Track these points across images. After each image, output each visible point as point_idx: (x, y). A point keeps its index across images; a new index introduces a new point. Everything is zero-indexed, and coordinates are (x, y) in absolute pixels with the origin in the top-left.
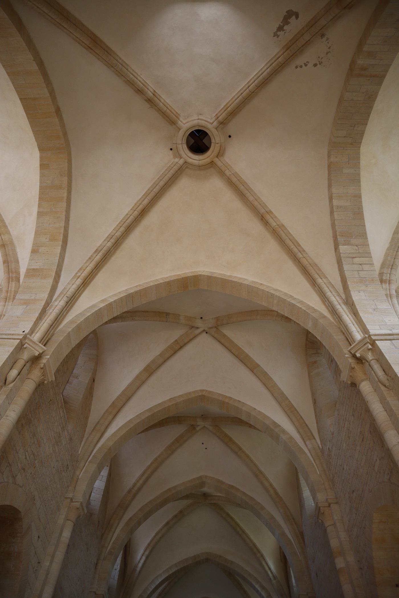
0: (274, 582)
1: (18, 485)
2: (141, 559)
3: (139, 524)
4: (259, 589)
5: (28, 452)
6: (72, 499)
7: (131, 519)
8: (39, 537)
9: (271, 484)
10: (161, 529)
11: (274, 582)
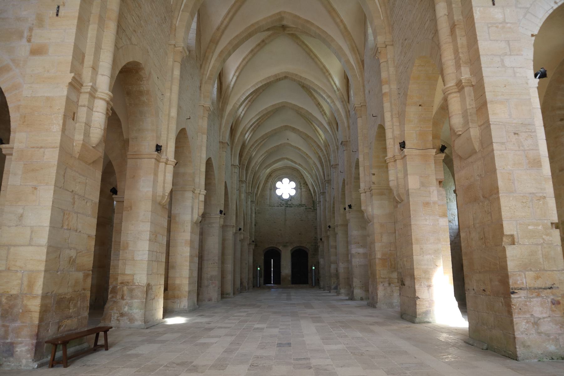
0: (337, 92)
1: (135, 44)
2: (233, 78)
3: (229, 55)
4: (326, 98)
5: (134, 16)
6: (175, 45)
7: (222, 51)
8: (158, 78)
9: (341, 20)
10: (247, 56)
11: (337, 92)
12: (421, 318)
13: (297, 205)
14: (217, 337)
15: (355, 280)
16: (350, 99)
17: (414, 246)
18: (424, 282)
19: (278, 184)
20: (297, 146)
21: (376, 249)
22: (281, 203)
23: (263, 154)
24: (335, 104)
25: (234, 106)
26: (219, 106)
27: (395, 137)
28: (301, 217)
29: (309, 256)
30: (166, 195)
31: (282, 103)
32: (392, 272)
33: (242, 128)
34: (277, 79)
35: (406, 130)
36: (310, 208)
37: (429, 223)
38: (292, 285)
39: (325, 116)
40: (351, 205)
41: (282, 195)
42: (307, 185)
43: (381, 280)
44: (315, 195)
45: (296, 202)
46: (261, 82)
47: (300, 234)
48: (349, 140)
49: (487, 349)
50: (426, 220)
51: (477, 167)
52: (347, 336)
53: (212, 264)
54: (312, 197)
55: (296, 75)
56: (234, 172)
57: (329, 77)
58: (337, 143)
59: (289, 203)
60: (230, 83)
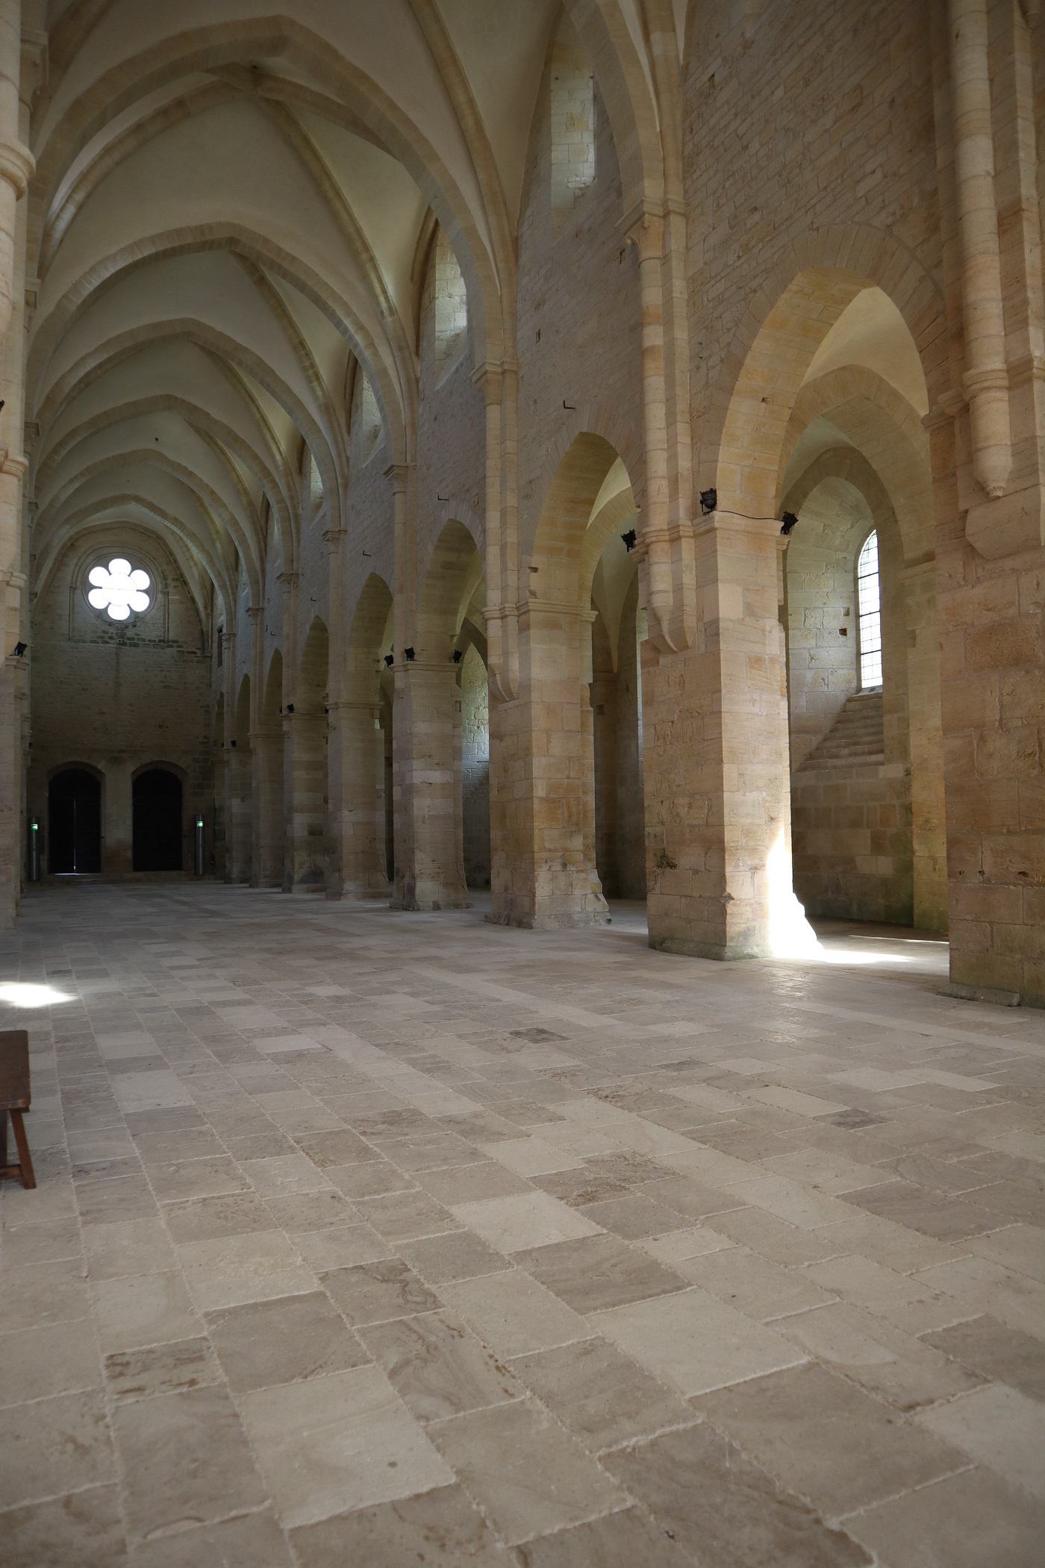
12: (736, 946)
13: (155, 641)
15: (419, 856)
17: (726, 767)
18: (744, 858)
19: (97, 575)
20: (184, 464)
21: (535, 774)
22: (105, 632)
23: (76, 477)
24: (376, 354)
25: (59, 305)
27: (679, 475)
28: (165, 677)
32: (572, 834)
34: (205, 243)
35: (720, 459)
36: (192, 652)
37: (760, 711)
38: (136, 873)
39: (315, 384)
40: (412, 649)
41: (107, 608)
42: (185, 583)
43: (545, 855)
44: (207, 615)
45: (152, 633)
46: (153, 239)
47: (161, 726)
48: (414, 464)
49: (1019, 1005)
50: (753, 702)
51: (1035, 582)
54: (200, 621)
55: (266, 241)
57: (368, 266)
59: (130, 633)
60: (54, 223)
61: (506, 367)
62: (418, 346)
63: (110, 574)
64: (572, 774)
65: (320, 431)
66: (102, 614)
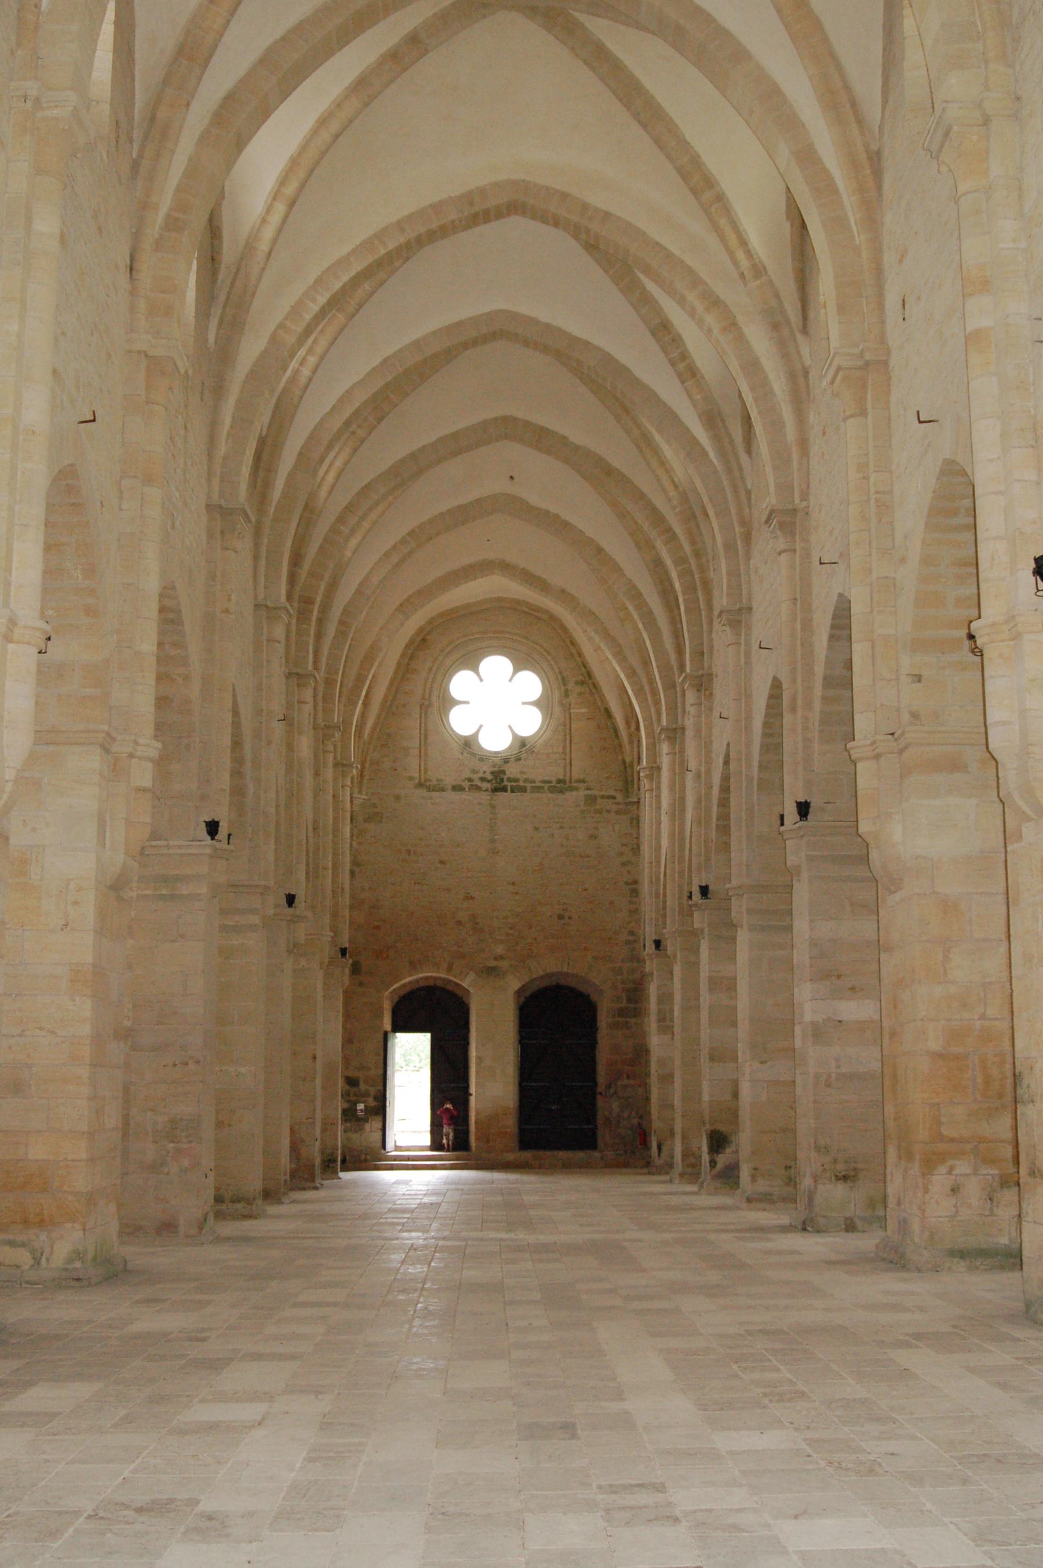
10: (339, 105)
13: (550, 782)
14: (255, 1397)
16: (811, 315)
22: (474, 772)
25: (274, 339)
26: (206, 340)
29: (603, 1020)
30: (7, 778)
31: (491, 316)
33: (306, 433)
34: (476, 216)
36: (608, 797)
44: (630, 735)
47: (560, 917)
52: (803, 1393)
53: (175, 1065)
55: (564, 196)
56: (268, 640)
58: (747, 511)
61: (868, 356)
62: (805, 317)
63: (481, 680)
64: (990, 1012)
65: (705, 453)
66: (469, 744)
